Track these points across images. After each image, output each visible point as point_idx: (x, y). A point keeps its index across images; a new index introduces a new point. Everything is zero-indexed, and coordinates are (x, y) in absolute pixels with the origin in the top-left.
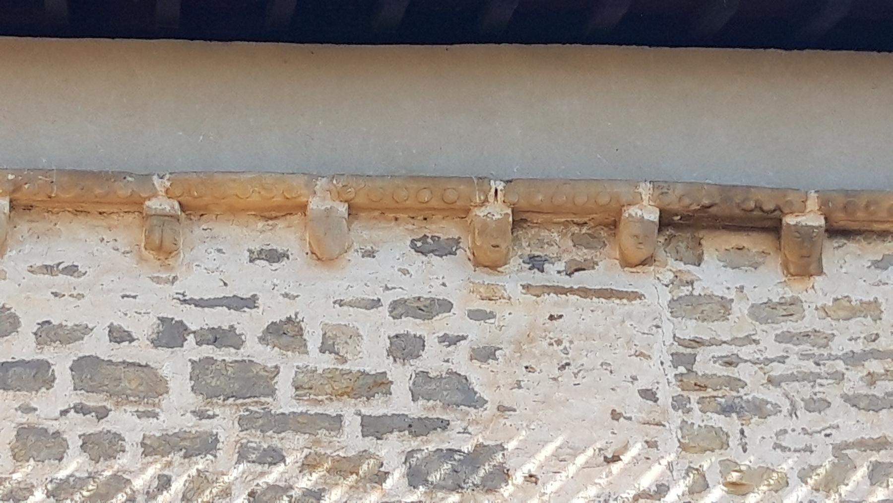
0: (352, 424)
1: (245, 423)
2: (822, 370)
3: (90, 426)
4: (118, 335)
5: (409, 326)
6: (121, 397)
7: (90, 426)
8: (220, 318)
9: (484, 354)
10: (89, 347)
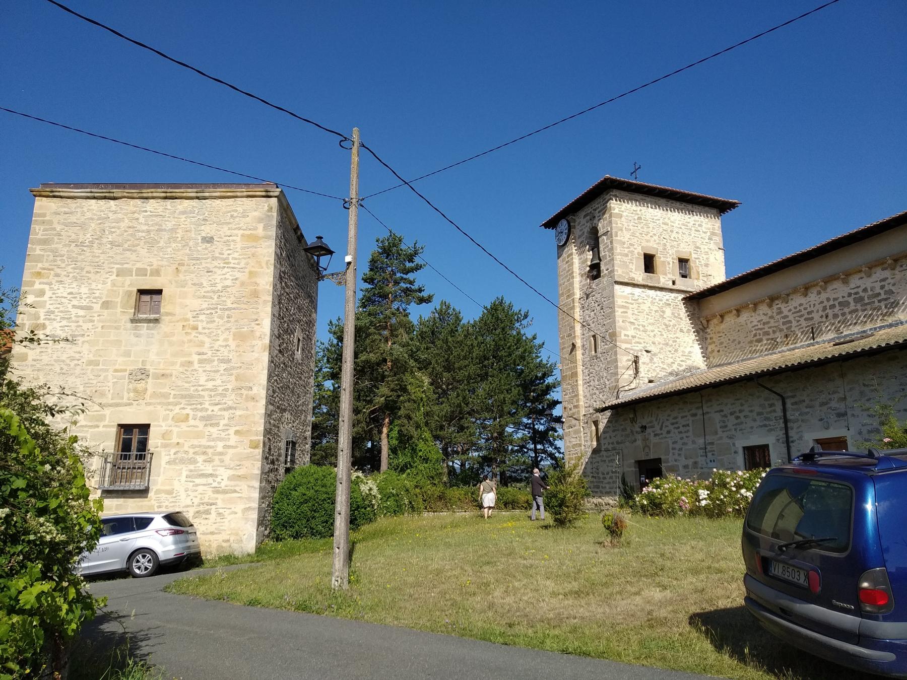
0: (876, 301)
1: (861, 306)
2: (754, 332)
3: (842, 312)
4: (843, 297)
5: (883, 283)
6: (845, 306)
7: (842, 312)
8: (856, 290)
9: (894, 285)
10: (841, 300)
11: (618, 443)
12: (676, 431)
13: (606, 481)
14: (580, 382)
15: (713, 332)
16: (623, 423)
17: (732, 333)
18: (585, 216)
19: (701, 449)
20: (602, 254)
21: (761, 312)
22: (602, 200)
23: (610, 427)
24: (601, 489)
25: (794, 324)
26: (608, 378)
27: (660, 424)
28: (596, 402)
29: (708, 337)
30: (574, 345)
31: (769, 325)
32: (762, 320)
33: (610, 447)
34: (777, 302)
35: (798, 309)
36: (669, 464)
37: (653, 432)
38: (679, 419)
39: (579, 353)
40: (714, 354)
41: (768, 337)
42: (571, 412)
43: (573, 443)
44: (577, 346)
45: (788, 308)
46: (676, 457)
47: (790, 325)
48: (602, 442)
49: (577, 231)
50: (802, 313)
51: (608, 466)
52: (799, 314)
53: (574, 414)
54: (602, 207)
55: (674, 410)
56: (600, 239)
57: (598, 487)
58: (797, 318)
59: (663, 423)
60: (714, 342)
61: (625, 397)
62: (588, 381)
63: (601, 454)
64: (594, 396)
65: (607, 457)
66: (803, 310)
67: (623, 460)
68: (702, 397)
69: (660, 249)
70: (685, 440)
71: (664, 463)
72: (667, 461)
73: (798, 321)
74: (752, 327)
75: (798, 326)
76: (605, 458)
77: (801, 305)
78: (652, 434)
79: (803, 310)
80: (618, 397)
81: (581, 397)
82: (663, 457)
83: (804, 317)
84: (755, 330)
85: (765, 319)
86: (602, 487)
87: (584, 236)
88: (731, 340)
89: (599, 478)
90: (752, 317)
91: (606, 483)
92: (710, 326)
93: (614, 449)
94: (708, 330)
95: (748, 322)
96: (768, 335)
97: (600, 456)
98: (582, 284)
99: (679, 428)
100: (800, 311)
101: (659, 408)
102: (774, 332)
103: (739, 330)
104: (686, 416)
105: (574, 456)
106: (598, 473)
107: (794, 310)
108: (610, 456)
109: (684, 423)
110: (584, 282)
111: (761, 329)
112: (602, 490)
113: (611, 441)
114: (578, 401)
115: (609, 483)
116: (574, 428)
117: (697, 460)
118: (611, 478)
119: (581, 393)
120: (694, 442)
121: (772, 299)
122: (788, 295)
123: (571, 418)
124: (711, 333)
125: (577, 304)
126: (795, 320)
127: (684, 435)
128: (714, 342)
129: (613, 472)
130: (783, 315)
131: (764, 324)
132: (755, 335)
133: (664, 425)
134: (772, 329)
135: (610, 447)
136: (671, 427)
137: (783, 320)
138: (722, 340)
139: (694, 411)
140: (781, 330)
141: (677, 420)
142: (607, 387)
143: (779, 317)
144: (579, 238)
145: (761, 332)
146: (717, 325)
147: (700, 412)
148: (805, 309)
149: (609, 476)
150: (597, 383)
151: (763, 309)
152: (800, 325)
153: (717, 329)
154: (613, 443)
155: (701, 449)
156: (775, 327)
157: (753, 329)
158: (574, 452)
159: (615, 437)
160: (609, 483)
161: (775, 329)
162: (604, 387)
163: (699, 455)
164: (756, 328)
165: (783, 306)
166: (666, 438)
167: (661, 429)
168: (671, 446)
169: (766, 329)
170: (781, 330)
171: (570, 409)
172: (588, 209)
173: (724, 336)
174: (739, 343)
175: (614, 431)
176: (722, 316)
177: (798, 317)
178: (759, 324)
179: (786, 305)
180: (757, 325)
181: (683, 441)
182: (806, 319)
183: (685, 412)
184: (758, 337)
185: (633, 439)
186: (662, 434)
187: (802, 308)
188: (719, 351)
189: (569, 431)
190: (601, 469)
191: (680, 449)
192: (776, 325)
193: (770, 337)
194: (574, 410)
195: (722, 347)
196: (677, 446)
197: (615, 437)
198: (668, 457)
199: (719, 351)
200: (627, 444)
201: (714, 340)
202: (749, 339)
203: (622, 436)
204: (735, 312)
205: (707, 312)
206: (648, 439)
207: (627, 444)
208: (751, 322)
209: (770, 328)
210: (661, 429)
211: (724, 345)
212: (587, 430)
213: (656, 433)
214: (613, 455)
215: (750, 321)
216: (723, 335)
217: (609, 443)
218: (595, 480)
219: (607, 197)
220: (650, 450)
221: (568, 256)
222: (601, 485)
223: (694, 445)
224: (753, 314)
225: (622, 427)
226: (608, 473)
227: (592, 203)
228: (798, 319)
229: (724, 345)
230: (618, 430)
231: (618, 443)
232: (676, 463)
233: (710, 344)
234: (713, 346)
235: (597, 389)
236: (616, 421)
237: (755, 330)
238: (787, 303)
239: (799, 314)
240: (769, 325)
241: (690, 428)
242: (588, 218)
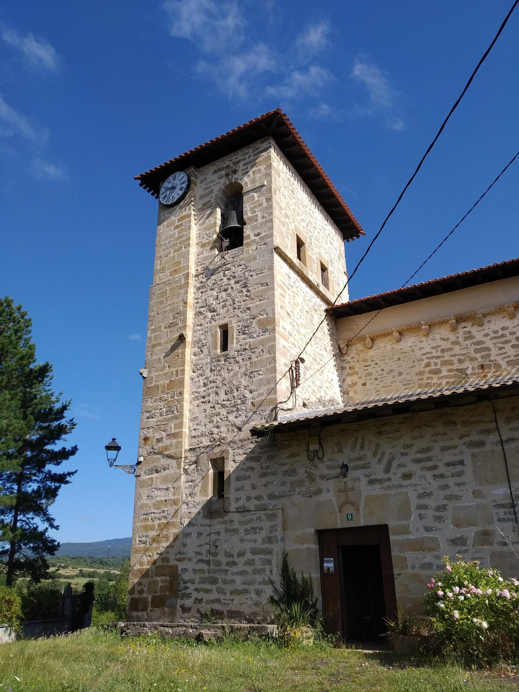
2: (426, 361)
11: (272, 497)
12: (429, 475)
13: (235, 569)
14: (187, 396)
15: (355, 360)
16: (286, 461)
17: (387, 361)
18: (215, 172)
19: (499, 506)
20: (247, 214)
21: (438, 337)
22: (251, 151)
23: (252, 469)
24: (220, 584)
25: (494, 351)
26: (252, 387)
27: (385, 462)
28: (218, 427)
29: (347, 366)
30: (182, 338)
31: (452, 353)
32: (439, 346)
33: (252, 505)
34: (464, 324)
35: (500, 334)
36: (411, 537)
37: (366, 476)
38: (436, 452)
39: (189, 351)
40: (355, 388)
41: (452, 367)
42: (160, 444)
43: (159, 499)
44: (187, 340)
45: (483, 333)
46: (429, 522)
47: (487, 352)
48: (231, 493)
49: (198, 190)
50: (507, 339)
51: (242, 540)
52: (503, 340)
53: (166, 448)
54: (252, 158)
55: (422, 437)
56: (245, 198)
57: (214, 581)
58: (498, 345)
59: (393, 459)
60: (357, 373)
61: (283, 417)
62: (202, 394)
63: (226, 518)
64: (215, 419)
65: (241, 523)
66: (508, 334)
67: (284, 529)
68: (495, 411)
69: (308, 240)
70: (455, 490)
71: (396, 533)
72: (405, 530)
73: (500, 349)
74: (424, 354)
75: (501, 354)
76: (236, 526)
77: (503, 329)
78: (364, 481)
79: (508, 334)
80: (276, 419)
81: (186, 420)
82: (392, 524)
83: (511, 344)
84: (427, 358)
85: (445, 345)
86: (225, 582)
87: (214, 195)
88: (386, 371)
89: (219, 564)
90: (422, 342)
91: (233, 574)
92: (349, 352)
93: (259, 508)
94: (346, 358)
95: (416, 349)
96: (451, 364)
97: (225, 522)
98: (201, 256)
99: (435, 467)
100: (503, 336)
101: (380, 433)
102: (460, 361)
103: (399, 359)
104: (455, 447)
105: (157, 522)
106: (215, 555)
107: (492, 335)
108: (251, 521)
109: (451, 459)
110: (206, 254)
111: (437, 357)
112: (224, 586)
113: (254, 494)
114: (180, 425)
115: (243, 573)
116: (163, 473)
117: (489, 528)
118: (250, 562)
119: (187, 414)
120: (476, 494)
121: (460, 319)
122: (484, 316)
123: (159, 456)
124: (352, 361)
125: (192, 281)
126: (495, 347)
127: (451, 482)
128: (357, 373)
129: (254, 552)
130: (474, 341)
131: (443, 351)
132: (428, 365)
133: (394, 464)
134: (457, 357)
135: (252, 505)
136: (415, 468)
137: (474, 347)
138: (370, 369)
139: (474, 438)
140: (472, 359)
141: (430, 454)
142: (249, 402)
143: (468, 342)
144: (200, 198)
145: (438, 361)
146: (362, 351)
147: (493, 438)
148: (512, 333)
149: (243, 560)
150: (223, 396)
151: (444, 332)
152: (505, 353)
153: (362, 356)
154: (258, 498)
155: (499, 506)
156: (463, 355)
157: (424, 357)
158: (157, 516)
159: (265, 486)
160: (243, 573)
161: (462, 357)
162: (239, 402)
163: (496, 518)
164: (430, 355)
165: (474, 330)
166: (400, 486)
167: (387, 470)
168: (414, 501)
169: (447, 358)
170: (472, 359)
171: (159, 440)
172: (226, 162)
173: (373, 364)
174: (400, 374)
175: (263, 475)
176: (373, 340)
177: (499, 343)
178: (434, 351)
179: (480, 328)
180: (431, 353)
181: (448, 492)
182: (513, 346)
183: (451, 439)
184: (433, 367)
185: (313, 489)
186: (389, 479)
187: (506, 332)
188: (364, 384)
189: (151, 479)
190: (225, 546)
191: (442, 508)
192: (465, 352)
193: (454, 367)
194: (167, 442)
195: (370, 379)
196: (431, 502)
197: (265, 486)
198: (404, 522)
199: (364, 384)
200: (297, 498)
201: (356, 370)
202: (418, 369)
203: (283, 484)
204: (396, 334)
205: (348, 334)
206: (353, 489)
207: (297, 498)
208: (421, 348)
209: (454, 356)
210: (387, 470)
211: (373, 377)
212: (197, 477)
213: (372, 477)
214: (259, 519)
215: (418, 347)
216: (373, 364)
217: (249, 499)
218: (205, 567)
219: (264, 145)
220: (357, 510)
221: (183, 218)
222: (220, 577)
223: (478, 501)
224: (424, 339)
225: (285, 468)
226: (241, 554)
227: (232, 155)
228: (501, 345)
229: (373, 377)
230: (274, 474)
231: (272, 497)
232: (431, 535)
233: (349, 375)
234: (355, 378)
235: (224, 406)
236: (271, 458)
237: (427, 358)
238: (481, 325)
239: (503, 340)
240: (452, 353)
241: (468, 469)
242: (223, 173)
